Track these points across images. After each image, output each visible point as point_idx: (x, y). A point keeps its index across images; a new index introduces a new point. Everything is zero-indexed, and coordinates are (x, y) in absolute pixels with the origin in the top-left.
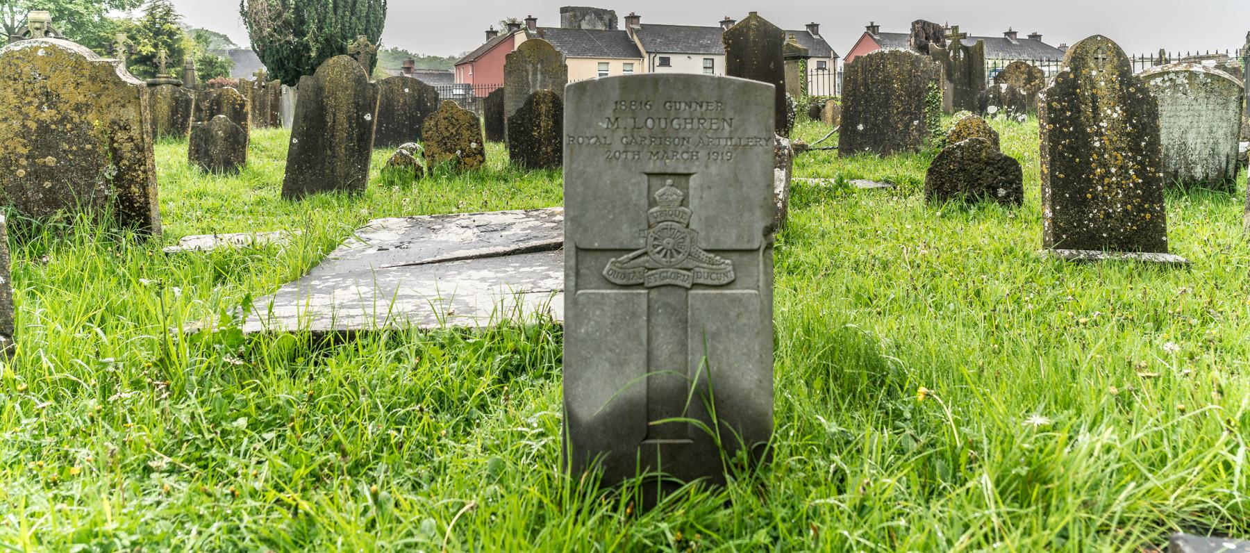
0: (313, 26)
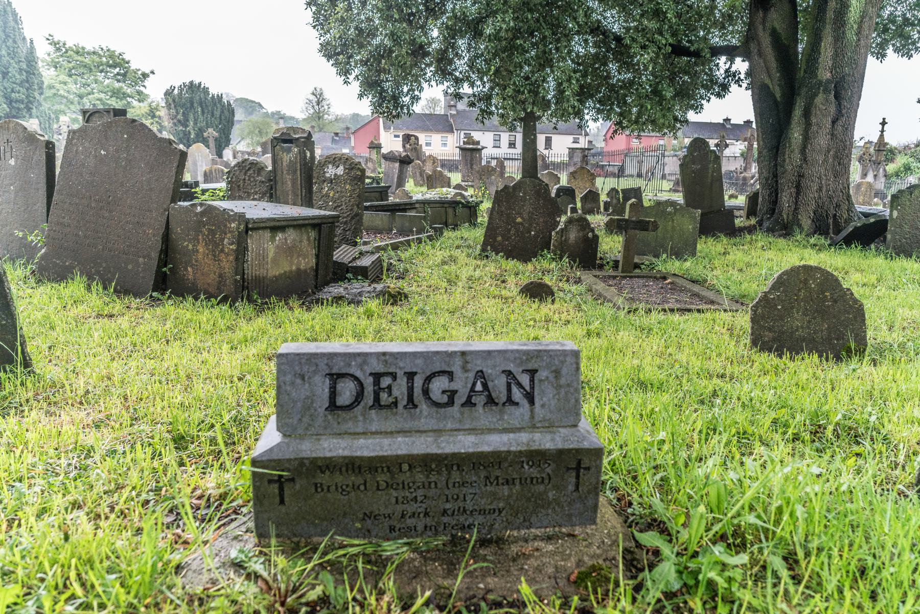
0: (192, 123)
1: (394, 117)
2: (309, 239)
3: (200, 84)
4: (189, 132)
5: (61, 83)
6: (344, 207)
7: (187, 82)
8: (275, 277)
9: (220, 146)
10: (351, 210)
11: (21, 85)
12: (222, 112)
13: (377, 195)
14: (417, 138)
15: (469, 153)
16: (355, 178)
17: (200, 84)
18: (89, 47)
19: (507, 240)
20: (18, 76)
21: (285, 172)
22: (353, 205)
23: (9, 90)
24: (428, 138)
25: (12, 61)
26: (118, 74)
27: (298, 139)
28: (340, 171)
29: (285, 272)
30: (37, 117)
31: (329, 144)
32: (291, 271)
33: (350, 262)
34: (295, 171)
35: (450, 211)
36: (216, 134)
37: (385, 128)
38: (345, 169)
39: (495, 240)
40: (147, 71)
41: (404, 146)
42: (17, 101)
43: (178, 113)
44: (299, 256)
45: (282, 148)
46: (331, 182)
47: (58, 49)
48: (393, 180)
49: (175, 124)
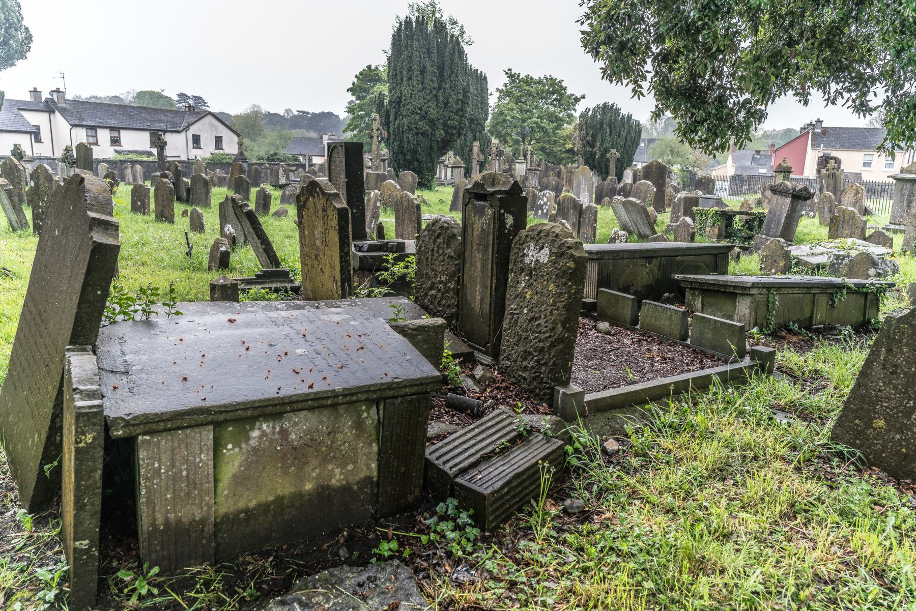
0: (598, 144)
1: (717, 149)
2: (359, 425)
3: (613, 105)
4: (595, 153)
5: (509, 109)
6: (542, 321)
7: (601, 103)
8: (246, 511)
9: (622, 166)
10: (553, 329)
11: (456, 113)
12: (629, 132)
13: (709, 259)
14: (838, 161)
15: (907, 186)
16: (564, 273)
17: (613, 105)
18: (536, 77)
19: (900, 431)
20: (455, 106)
21: (475, 247)
22: (555, 322)
23: (447, 118)
24: (868, 158)
25: (452, 93)
26: (556, 100)
27: (494, 193)
28: (544, 256)
29: (279, 500)
30: (479, 140)
31: (748, 163)
32: (301, 495)
33: (463, 471)
34: (487, 247)
35: (823, 300)
36: (618, 154)
37: (813, 145)
38: (551, 253)
39: (869, 425)
40: (579, 96)
41: (819, 172)
42: (452, 127)
43: (587, 134)
44: (325, 460)
45: (475, 206)
46: (530, 274)
47: (514, 81)
48: (779, 221)
49: (584, 145)
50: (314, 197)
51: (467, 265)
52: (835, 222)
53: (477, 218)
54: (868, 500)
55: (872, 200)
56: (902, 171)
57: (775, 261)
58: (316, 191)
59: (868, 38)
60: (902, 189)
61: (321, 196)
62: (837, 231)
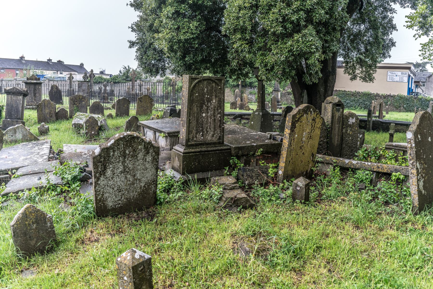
15: (32, 86)
21: (336, 123)
45: (336, 108)
50: (308, 114)
51: (333, 130)
52: (40, 106)
53: (337, 112)
54: (202, 201)
55: (160, 94)
56: (28, 79)
57: (93, 127)
58: (310, 111)
59: (358, 41)
60: (30, 88)
61: (313, 113)
62: (42, 111)
